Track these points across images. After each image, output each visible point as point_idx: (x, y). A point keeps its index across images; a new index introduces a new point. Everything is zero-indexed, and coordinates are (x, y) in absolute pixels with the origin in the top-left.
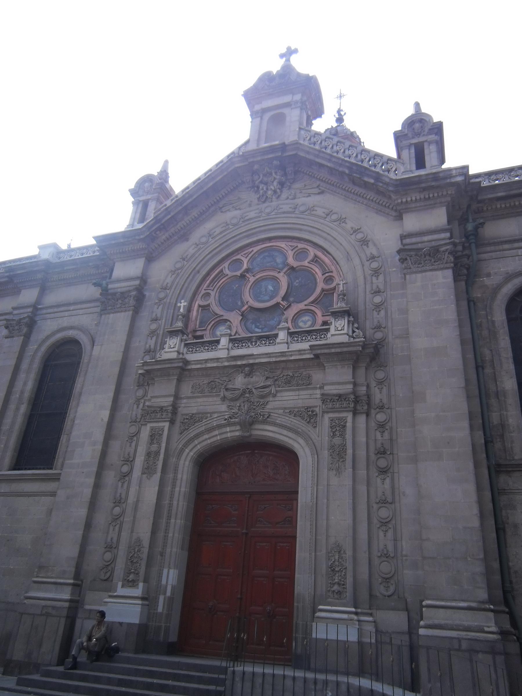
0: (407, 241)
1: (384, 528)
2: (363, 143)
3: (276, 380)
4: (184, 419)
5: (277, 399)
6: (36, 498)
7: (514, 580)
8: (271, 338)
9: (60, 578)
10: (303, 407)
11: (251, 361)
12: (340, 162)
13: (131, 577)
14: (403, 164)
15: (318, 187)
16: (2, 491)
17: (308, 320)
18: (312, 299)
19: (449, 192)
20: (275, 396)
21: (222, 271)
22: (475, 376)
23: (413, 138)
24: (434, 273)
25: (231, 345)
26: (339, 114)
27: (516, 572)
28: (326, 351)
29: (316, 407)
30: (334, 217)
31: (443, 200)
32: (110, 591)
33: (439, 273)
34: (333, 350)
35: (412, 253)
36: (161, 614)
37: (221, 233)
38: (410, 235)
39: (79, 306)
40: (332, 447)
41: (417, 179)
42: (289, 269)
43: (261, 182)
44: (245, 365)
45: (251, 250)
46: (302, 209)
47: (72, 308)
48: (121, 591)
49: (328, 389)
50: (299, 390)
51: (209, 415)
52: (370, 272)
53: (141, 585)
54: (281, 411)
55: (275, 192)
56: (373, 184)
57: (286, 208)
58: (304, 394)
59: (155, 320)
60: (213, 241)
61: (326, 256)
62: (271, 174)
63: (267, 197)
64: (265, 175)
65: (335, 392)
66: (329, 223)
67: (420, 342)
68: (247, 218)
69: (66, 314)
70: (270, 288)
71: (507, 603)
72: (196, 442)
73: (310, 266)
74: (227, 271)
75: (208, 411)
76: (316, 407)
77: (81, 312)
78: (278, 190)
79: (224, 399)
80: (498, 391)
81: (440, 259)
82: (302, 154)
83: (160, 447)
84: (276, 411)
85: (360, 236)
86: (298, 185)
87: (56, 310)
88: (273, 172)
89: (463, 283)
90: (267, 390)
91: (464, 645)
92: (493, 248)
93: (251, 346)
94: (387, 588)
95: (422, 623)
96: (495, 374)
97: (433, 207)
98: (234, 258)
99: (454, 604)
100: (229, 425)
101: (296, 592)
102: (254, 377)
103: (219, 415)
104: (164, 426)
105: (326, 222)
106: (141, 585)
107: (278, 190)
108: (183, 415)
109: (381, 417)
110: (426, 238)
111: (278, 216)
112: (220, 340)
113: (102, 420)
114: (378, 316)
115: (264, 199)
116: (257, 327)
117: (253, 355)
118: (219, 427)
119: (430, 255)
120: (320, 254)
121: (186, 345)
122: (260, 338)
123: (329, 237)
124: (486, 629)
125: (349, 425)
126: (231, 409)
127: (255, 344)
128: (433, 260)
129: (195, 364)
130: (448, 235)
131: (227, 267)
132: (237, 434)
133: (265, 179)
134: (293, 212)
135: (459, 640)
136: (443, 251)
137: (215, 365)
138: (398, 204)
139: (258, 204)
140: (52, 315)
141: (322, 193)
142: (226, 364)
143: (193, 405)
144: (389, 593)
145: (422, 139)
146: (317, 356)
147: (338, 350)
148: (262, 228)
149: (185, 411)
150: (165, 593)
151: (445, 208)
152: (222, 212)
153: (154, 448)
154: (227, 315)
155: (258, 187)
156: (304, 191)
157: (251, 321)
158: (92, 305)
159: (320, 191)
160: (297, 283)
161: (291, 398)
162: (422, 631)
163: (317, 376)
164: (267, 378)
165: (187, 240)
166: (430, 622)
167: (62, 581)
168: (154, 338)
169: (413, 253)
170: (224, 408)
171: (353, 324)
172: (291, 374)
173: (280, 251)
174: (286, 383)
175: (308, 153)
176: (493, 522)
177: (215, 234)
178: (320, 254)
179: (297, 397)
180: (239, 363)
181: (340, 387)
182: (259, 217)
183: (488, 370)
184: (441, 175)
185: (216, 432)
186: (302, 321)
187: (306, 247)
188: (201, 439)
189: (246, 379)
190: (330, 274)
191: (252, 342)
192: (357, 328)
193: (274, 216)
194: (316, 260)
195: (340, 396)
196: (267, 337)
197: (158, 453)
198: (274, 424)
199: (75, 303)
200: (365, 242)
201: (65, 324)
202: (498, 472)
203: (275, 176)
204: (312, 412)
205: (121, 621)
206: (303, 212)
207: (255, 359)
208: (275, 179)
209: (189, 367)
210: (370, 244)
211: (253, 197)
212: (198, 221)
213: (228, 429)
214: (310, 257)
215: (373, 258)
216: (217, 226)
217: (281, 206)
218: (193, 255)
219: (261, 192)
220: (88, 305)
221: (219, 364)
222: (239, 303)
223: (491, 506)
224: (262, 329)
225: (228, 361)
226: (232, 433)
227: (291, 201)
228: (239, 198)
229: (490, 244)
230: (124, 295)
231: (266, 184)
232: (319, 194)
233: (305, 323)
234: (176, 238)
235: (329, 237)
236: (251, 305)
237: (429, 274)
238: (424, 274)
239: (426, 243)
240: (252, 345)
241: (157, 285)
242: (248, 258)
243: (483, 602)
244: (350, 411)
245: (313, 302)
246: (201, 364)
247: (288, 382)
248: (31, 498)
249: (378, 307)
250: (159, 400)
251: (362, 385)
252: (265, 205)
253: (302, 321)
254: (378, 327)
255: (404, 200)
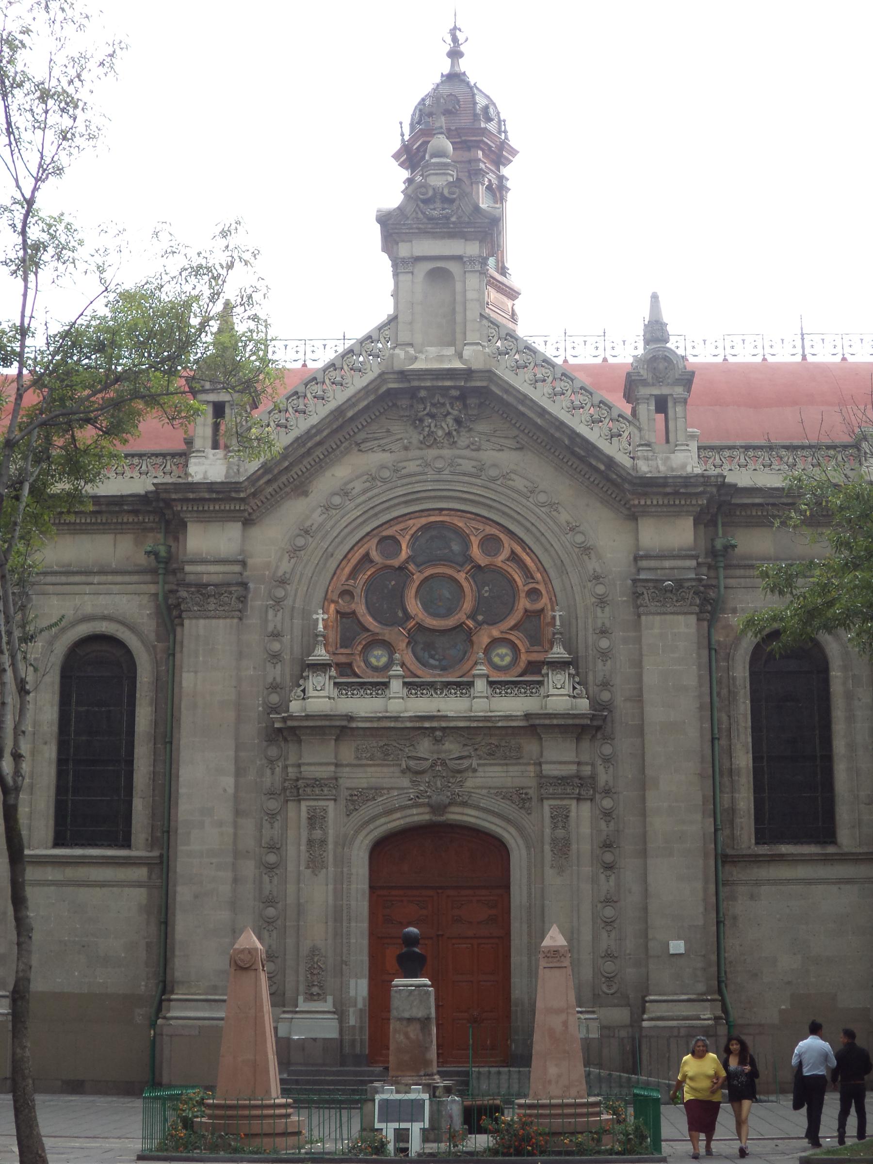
0: (644, 564)
1: (609, 928)
2: (504, 121)
3: (476, 750)
4: (351, 795)
5: (478, 774)
6: (115, 889)
7: (728, 970)
8: (464, 686)
9: (211, 995)
10: (512, 788)
11: (444, 724)
12: (557, 423)
13: (315, 990)
14: (640, 430)
15: (514, 437)
16: (50, 878)
17: (506, 655)
18: (511, 622)
19: (700, 502)
20: (475, 771)
21: (367, 555)
22: (710, 752)
23: (653, 385)
24: (676, 617)
25: (405, 690)
26: (455, 39)
27: (731, 962)
28: (547, 722)
29: (530, 788)
30: (542, 498)
31: (691, 509)
32: (284, 1006)
33: (681, 618)
34: (555, 722)
35: (650, 584)
36: (354, 1026)
37: (364, 492)
38: (647, 557)
39: (110, 578)
40: (554, 841)
41: (661, 481)
42: (473, 567)
43: (427, 414)
44: (433, 729)
45: (411, 522)
46: (493, 473)
47: (96, 579)
48: (302, 1006)
49: (547, 769)
50: (507, 765)
51: (385, 791)
52: (594, 600)
53: (330, 999)
54: (484, 792)
55: (449, 434)
56: (603, 472)
57: (467, 466)
58: (514, 770)
59: (276, 635)
60: (352, 505)
61: (527, 554)
62: (443, 404)
63: (435, 439)
64: (433, 405)
65: (556, 773)
66: (535, 508)
67: (656, 713)
68: (404, 472)
69: (87, 589)
70: (446, 594)
71: (720, 992)
72: (372, 826)
73: (505, 567)
74: (375, 555)
75: (385, 786)
76: (530, 788)
77: (115, 588)
78: (454, 433)
79: (403, 772)
80: (731, 769)
81: (683, 599)
82: (494, 389)
83: (326, 833)
84: (477, 791)
85: (579, 538)
86: (482, 427)
87: (63, 579)
88: (447, 402)
89: (705, 624)
90: (466, 763)
91: (683, 1032)
92: (741, 572)
93: (434, 695)
94: (609, 987)
95: (645, 1016)
96: (730, 746)
97: (678, 515)
98: (384, 534)
99: (675, 998)
100: (417, 805)
101: (512, 997)
102: (447, 743)
103: (401, 792)
104: (327, 806)
105: (528, 503)
106: (330, 999)
107: (454, 433)
108: (347, 789)
109: (607, 803)
110: (667, 564)
111: (456, 478)
112: (389, 682)
113: (225, 790)
114: (604, 668)
115: (429, 441)
116: (432, 657)
117: (446, 716)
118: (402, 808)
119: (672, 591)
120: (518, 550)
121: (335, 684)
122: (447, 685)
123: (533, 529)
124: (702, 1017)
125: (573, 814)
126: (417, 785)
127: (441, 693)
128: (675, 599)
129: (363, 721)
130: (693, 563)
131: (374, 547)
132: (427, 817)
133: (434, 410)
134: (478, 477)
135: (679, 1028)
136: (688, 588)
137: (392, 725)
138: (634, 506)
139: (421, 449)
140: (59, 588)
141: (521, 449)
142: (409, 725)
143: (361, 775)
144: (612, 991)
145: (665, 391)
146: (533, 727)
147: (562, 722)
148: (432, 494)
149: (349, 783)
150: (355, 1006)
151: (692, 518)
152: (360, 451)
153: (318, 834)
154: (387, 634)
155: (421, 420)
156: (493, 439)
157: (422, 646)
158: (135, 578)
159: (518, 446)
160: (486, 591)
161: (497, 774)
162: (645, 1024)
163: (531, 748)
164: (465, 745)
165: (306, 494)
166: (653, 1015)
167: (217, 997)
168: (278, 667)
169: (650, 584)
170: (405, 782)
171: (573, 678)
172: (496, 743)
173: (456, 530)
174: (490, 754)
175: (506, 391)
176: (715, 916)
177: (355, 492)
178: (518, 550)
179: (504, 774)
180: (427, 725)
181: (563, 767)
182: (425, 474)
183: (724, 742)
184: (692, 480)
185: (398, 815)
186: (498, 655)
187: (497, 532)
188: (378, 823)
189: (436, 747)
190: (534, 585)
191: (436, 689)
192: (578, 683)
193: (450, 477)
194: (514, 557)
195: (563, 778)
196: (458, 684)
197: (323, 842)
198: (477, 807)
199: (101, 572)
200: (586, 550)
201: (89, 609)
202: (724, 863)
203: (450, 410)
204: (526, 794)
205: (314, 1037)
206: (493, 480)
207: (449, 721)
208: (448, 413)
209: (354, 725)
210: (593, 555)
211: (415, 437)
212: (320, 466)
213: (415, 811)
214: (505, 554)
215: (597, 578)
216: (357, 477)
217: (460, 461)
218: (321, 525)
219: (427, 429)
220: (127, 578)
221: (399, 725)
222: (400, 614)
223: (714, 899)
224: (439, 660)
225: (411, 721)
226: (419, 816)
227: (474, 454)
228: (388, 431)
229: (739, 567)
230: (222, 587)
231: (433, 416)
232: (517, 449)
233: (502, 658)
234: (288, 489)
235: (543, 539)
236: (419, 621)
237: (668, 617)
238: (663, 617)
239: (667, 571)
240: (436, 693)
241: (267, 573)
242: (408, 537)
243: (702, 994)
244: (574, 798)
245: (511, 629)
246: (371, 721)
247: (491, 754)
248: (105, 890)
249: (605, 655)
250: (312, 768)
251: (587, 764)
252: (432, 453)
253: (498, 655)
254: (605, 685)
255: (642, 502)
